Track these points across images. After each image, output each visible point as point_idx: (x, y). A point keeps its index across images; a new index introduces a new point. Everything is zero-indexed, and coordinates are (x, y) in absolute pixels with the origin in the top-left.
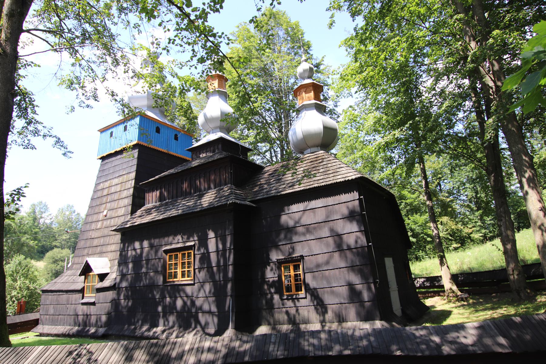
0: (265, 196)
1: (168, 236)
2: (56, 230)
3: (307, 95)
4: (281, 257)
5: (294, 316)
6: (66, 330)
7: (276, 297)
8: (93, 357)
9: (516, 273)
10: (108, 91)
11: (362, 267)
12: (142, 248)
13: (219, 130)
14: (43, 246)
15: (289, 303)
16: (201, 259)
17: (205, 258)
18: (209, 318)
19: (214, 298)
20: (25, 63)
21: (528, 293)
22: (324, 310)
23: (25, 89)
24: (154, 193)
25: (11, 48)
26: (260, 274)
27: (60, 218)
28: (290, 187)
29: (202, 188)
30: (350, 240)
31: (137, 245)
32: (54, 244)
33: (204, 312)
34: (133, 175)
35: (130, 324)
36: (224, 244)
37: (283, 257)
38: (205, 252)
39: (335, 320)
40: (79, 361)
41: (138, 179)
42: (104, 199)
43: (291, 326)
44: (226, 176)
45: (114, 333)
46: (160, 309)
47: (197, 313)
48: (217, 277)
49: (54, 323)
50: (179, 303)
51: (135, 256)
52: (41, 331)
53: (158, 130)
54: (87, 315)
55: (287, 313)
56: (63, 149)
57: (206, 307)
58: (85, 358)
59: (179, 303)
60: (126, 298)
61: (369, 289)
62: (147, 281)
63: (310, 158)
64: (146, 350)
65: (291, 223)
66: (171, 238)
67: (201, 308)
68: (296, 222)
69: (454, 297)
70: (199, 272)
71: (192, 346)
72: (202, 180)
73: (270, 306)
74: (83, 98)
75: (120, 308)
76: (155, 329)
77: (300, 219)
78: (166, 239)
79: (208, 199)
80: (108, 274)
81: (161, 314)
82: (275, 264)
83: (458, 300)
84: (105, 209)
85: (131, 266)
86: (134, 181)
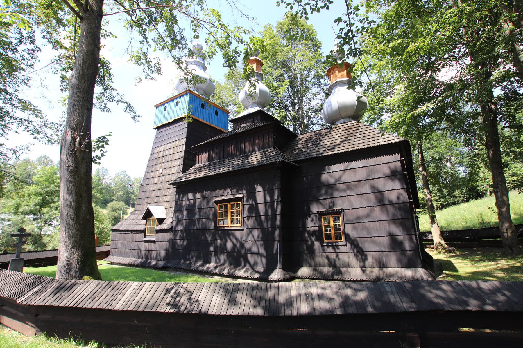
0: (307, 157)
1: (219, 189)
2: (114, 188)
3: (340, 73)
4: (322, 209)
5: (335, 261)
6: (131, 261)
7: (317, 244)
8: (193, 296)
9: (510, 231)
10: (175, 59)
11: (403, 220)
12: (195, 199)
13: (256, 105)
14: (105, 199)
15: (330, 250)
16: (249, 209)
17: (253, 209)
18: (258, 259)
19: (262, 242)
20: (105, 33)
21: (520, 248)
22: (364, 257)
23: (104, 58)
24: (203, 155)
25: (97, 6)
26: (301, 223)
27: (117, 180)
28: (330, 149)
29: (247, 150)
30: (393, 196)
31: (190, 196)
32: (112, 198)
33: (252, 254)
34: (184, 141)
35: (186, 260)
36: (272, 197)
37: (324, 210)
38: (254, 203)
39: (375, 265)
40: (179, 301)
41: (187, 144)
42: (160, 160)
43: (331, 268)
44: (269, 140)
45: (172, 265)
46: (212, 249)
47: (246, 254)
48: (265, 225)
49: (121, 255)
50: (229, 245)
51: (189, 205)
52: (112, 261)
53: (203, 106)
54: (149, 250)
55: (327, 257)
56: (132, 113)
57: (255, 249)
58: (184, 297)
59: (229, 245)
60: (182, 238)
61: (411, 240)
62: (200, 226)
63: (344, 126)
64: (248, 293)
65: (332, 181)
66: (221, 191)
67: (249, 250)
68: (337, 180)
69: (442, 249)
70: (248, 220)
71: (298, 292)
72: (247, 144)
73: (312, 251)
74: (148, 72)
75: (177, 246)
76: (208, 265)
77: (340, 177)
78: (217, 192)
79: (255, 159)
80: (165, 219)
81: (213, 253)
82: (316, 216)
83: (446, 252)
84: (161, 168)
85: (185, 213)
86: (184, 146)
